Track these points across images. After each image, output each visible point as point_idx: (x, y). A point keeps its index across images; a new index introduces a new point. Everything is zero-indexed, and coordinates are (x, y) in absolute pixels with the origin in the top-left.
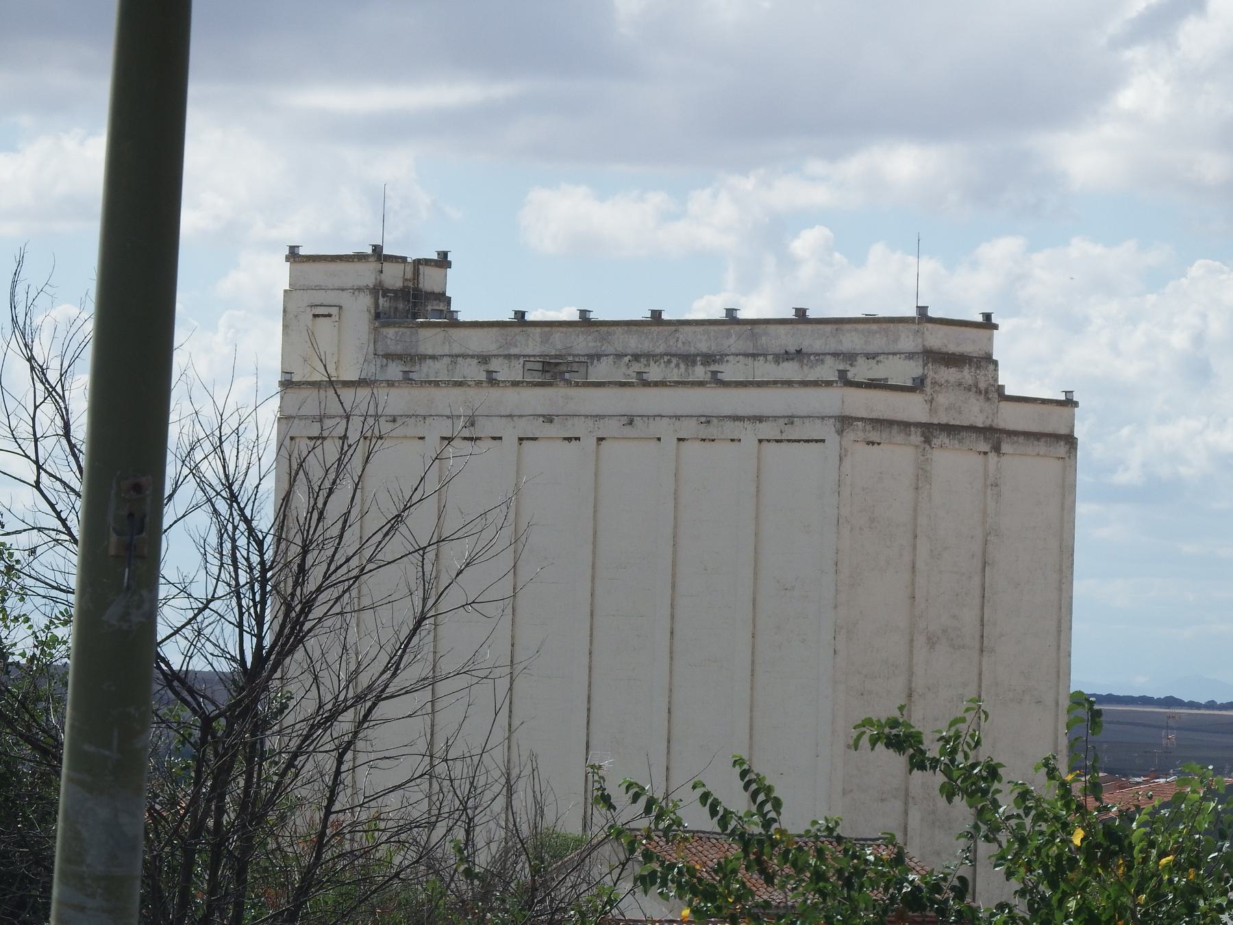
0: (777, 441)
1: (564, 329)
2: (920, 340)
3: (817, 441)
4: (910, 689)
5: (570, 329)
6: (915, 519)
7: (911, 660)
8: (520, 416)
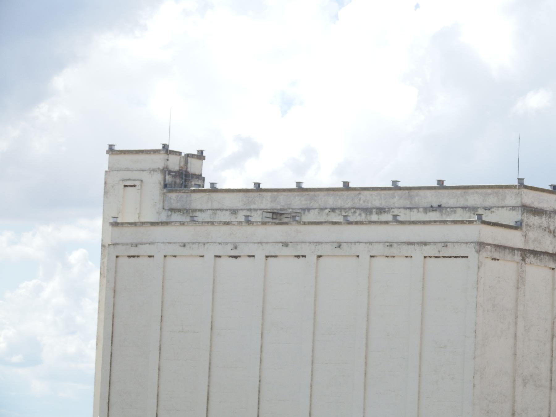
0: (436, 257)
3: (463, 257)
4: (513, 410)
5: (290, 194)
6: (517, 306)
7: (514, 392)
8: (267, 243)
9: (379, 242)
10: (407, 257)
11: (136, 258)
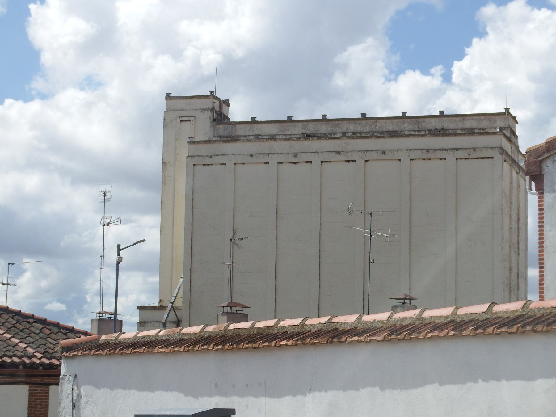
0: (466, 159)
1: (315, 123)
2: (507, 122)
3: (488, 158)
5: (318, 123)
8: (321, 152)
9: (418, 150)
10: (441, 159)
11: (210, 166)
